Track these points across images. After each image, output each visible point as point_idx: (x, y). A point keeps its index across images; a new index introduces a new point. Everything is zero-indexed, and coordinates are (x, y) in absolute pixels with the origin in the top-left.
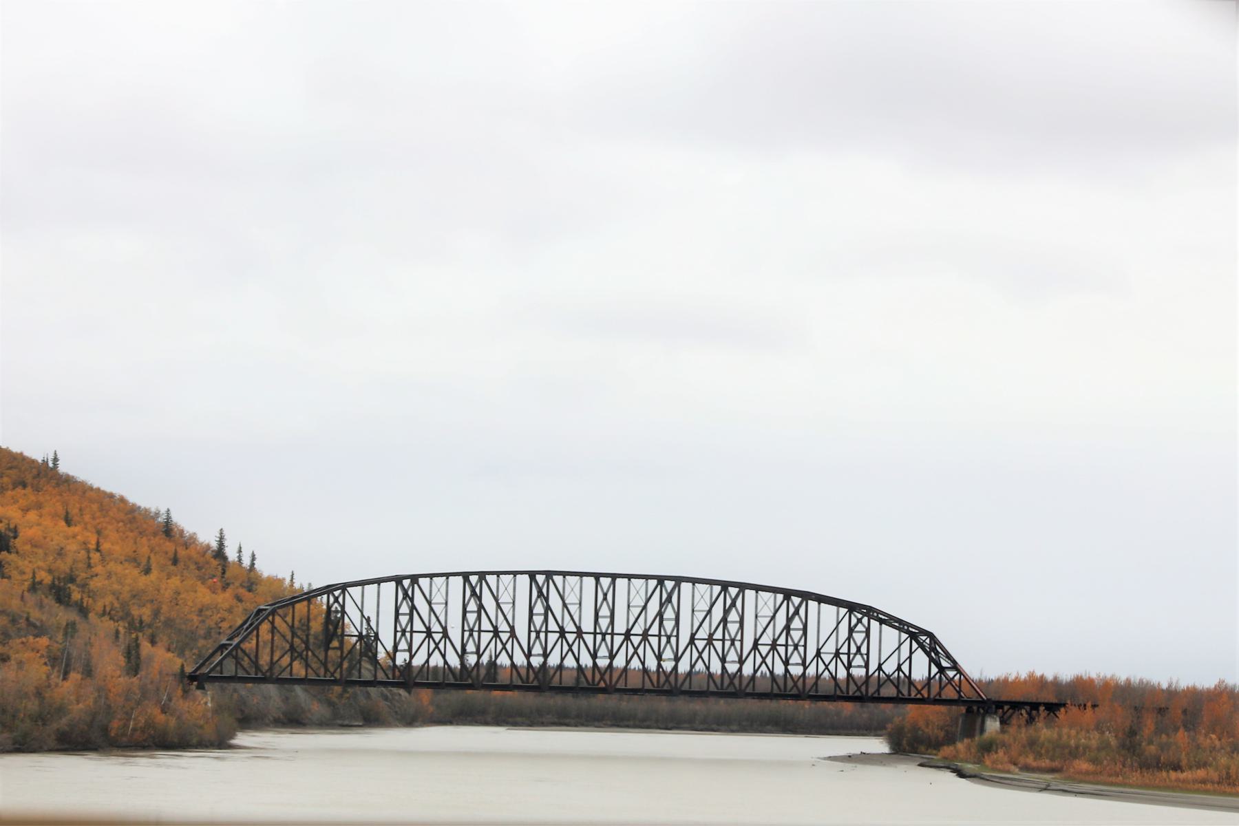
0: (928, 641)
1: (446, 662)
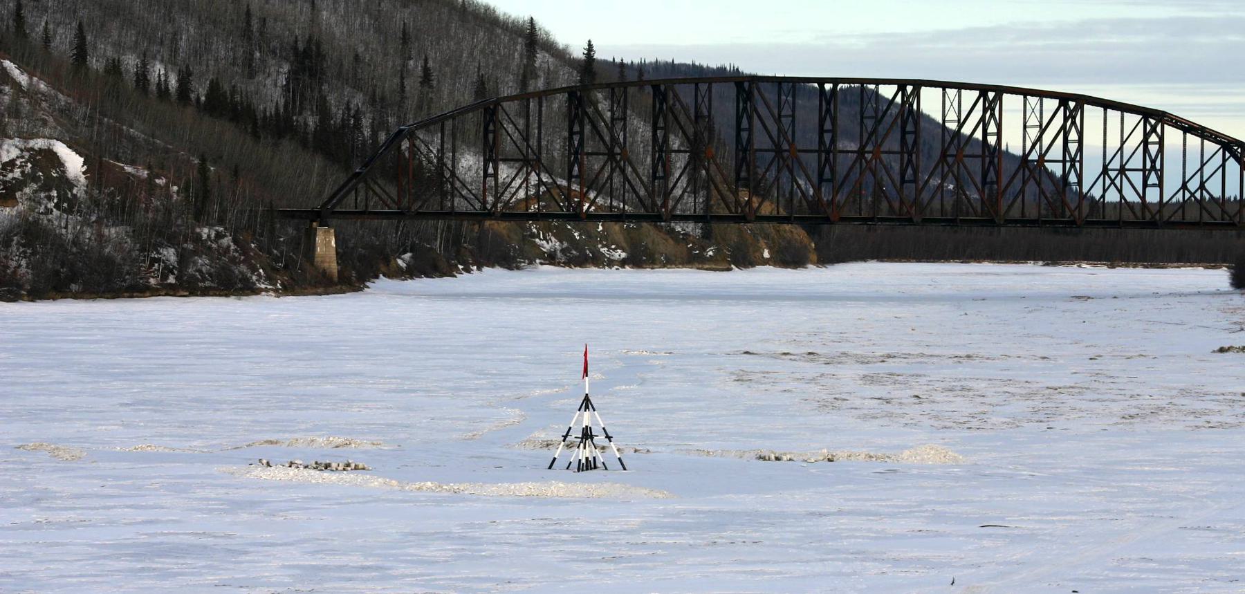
0: (1239, 150)
1: (1122, 197)
